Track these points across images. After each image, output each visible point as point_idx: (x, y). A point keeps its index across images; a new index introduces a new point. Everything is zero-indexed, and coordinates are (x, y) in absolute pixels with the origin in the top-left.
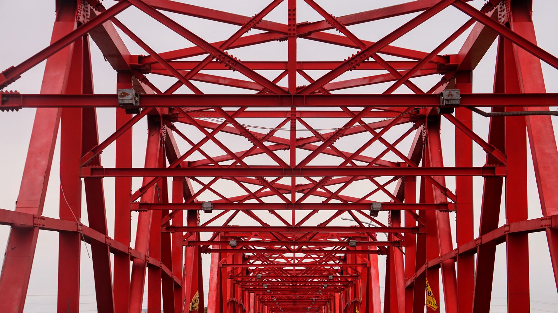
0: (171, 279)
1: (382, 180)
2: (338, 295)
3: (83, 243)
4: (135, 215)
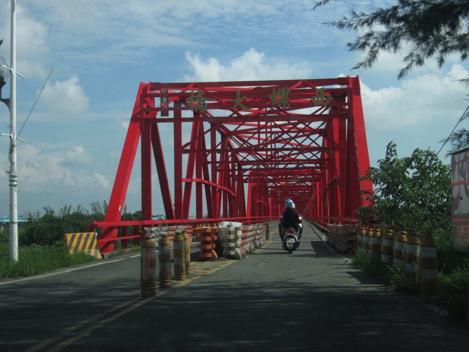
0: (231, 194)
1: (315, 153)
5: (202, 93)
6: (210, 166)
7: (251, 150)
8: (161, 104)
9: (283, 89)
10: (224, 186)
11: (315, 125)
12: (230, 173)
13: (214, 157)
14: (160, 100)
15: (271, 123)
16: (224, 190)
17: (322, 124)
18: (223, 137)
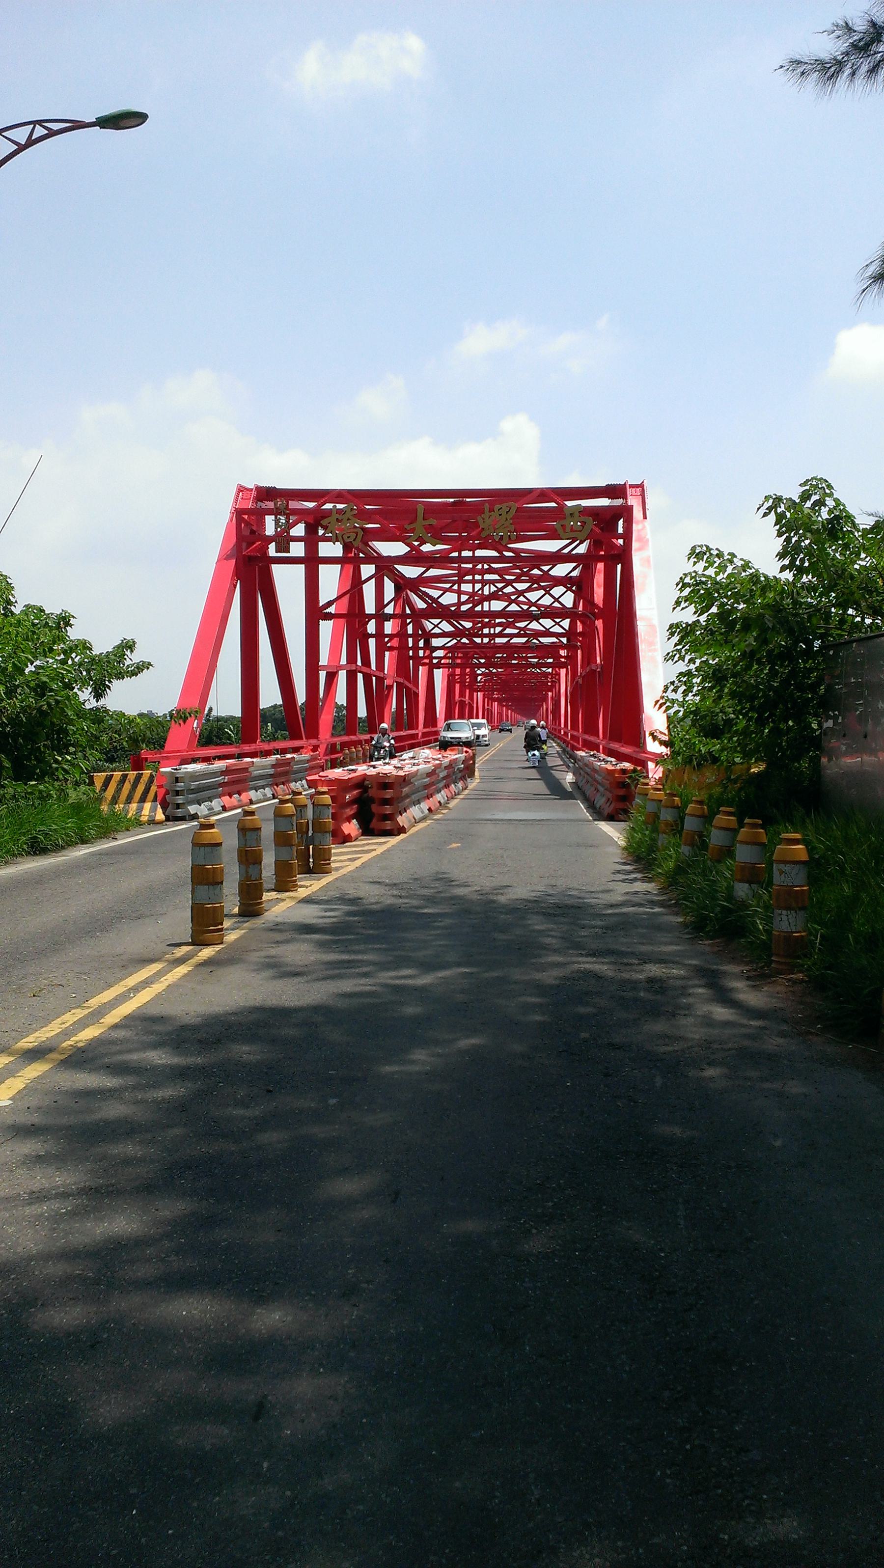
2: (563, 671)
3: (359, 674)
4: (387, 654)
5: (352, 509)
6: (372, 642)
7: (444, 613)
8: (276, 528)
9: (504, 506)
11: (561, 570)
12: (409, 654)
13: (380, 627)
14: (274, 522)
15: (483, 566)
17: (574, 569)
18: (398, 589)
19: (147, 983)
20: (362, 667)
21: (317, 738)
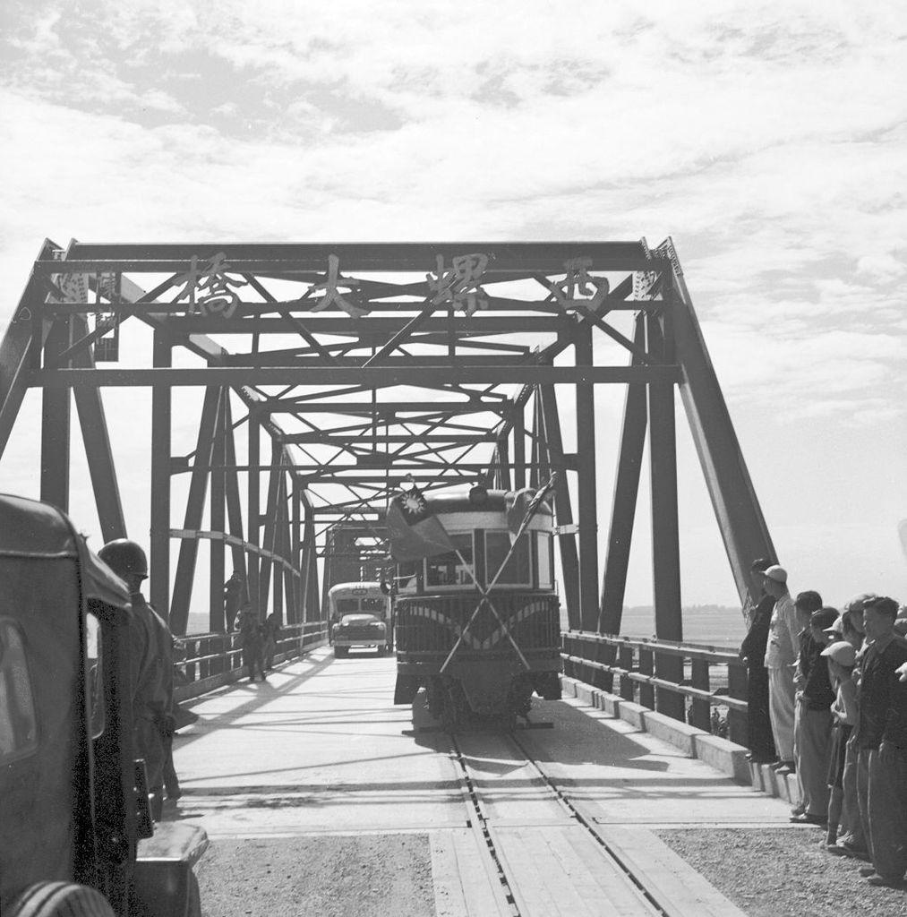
10: (275, 552)
16: (276, 562)
19: (594, 792)
20: (249, 545)
21: (778, 564)
